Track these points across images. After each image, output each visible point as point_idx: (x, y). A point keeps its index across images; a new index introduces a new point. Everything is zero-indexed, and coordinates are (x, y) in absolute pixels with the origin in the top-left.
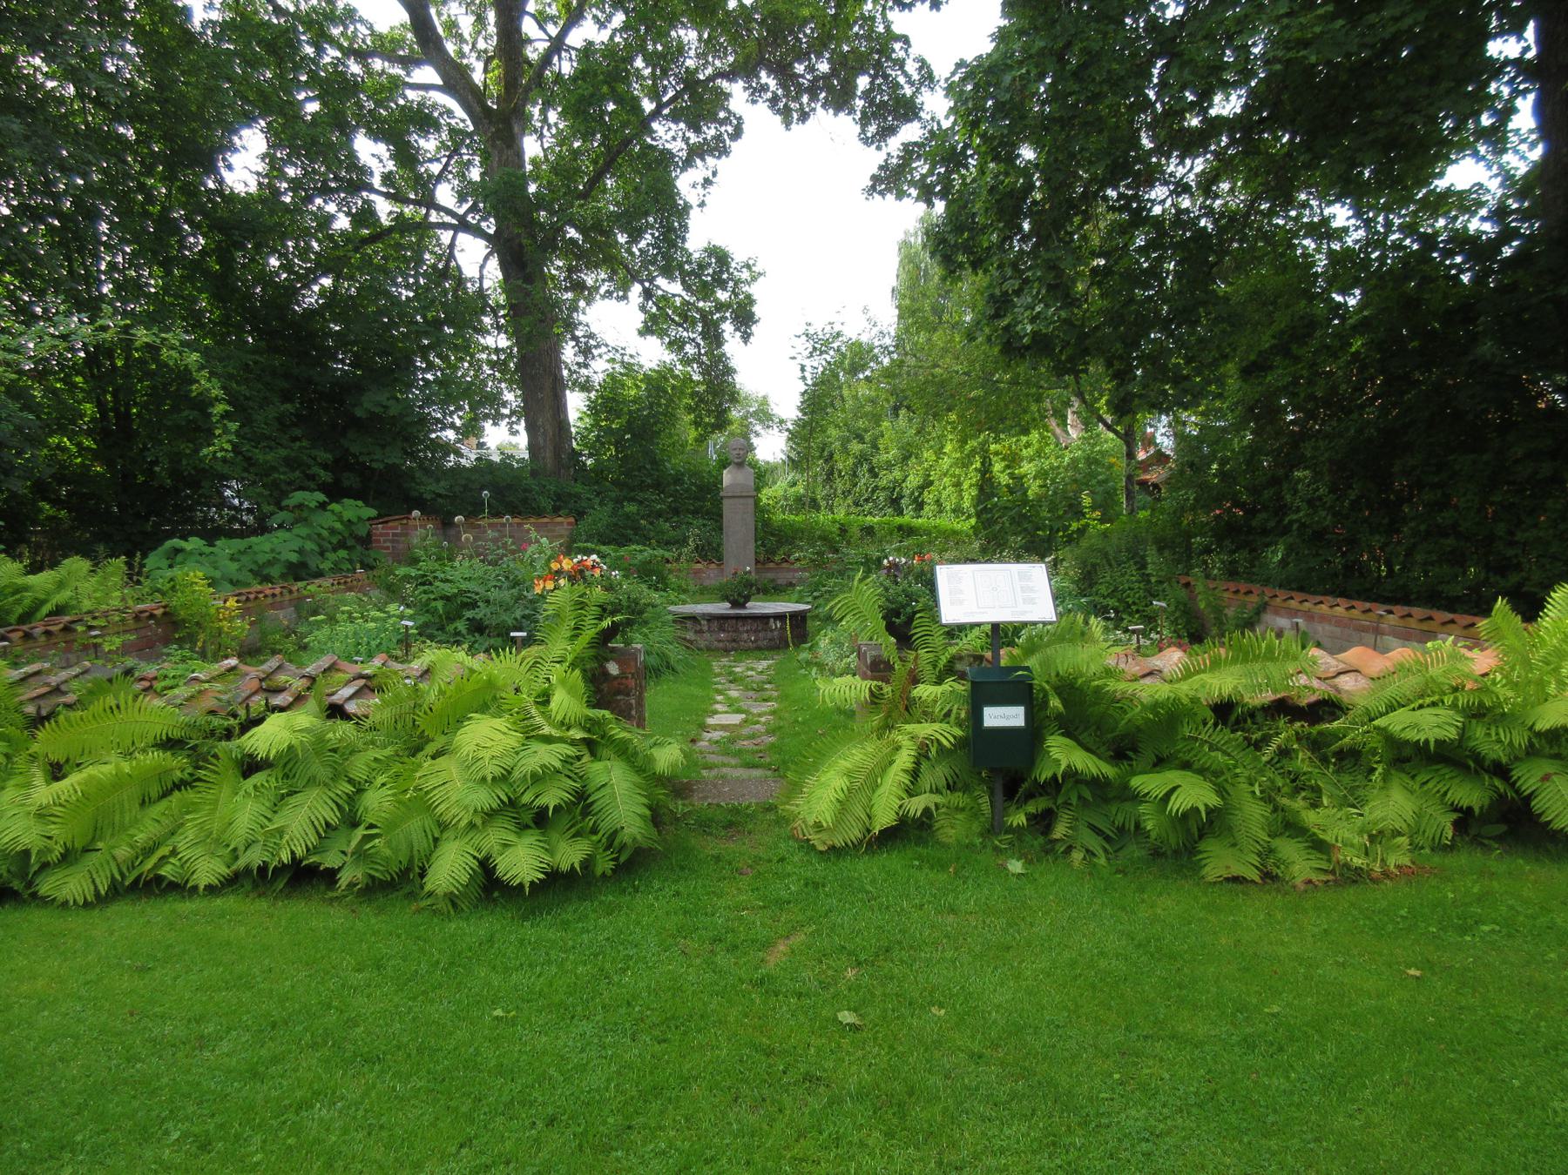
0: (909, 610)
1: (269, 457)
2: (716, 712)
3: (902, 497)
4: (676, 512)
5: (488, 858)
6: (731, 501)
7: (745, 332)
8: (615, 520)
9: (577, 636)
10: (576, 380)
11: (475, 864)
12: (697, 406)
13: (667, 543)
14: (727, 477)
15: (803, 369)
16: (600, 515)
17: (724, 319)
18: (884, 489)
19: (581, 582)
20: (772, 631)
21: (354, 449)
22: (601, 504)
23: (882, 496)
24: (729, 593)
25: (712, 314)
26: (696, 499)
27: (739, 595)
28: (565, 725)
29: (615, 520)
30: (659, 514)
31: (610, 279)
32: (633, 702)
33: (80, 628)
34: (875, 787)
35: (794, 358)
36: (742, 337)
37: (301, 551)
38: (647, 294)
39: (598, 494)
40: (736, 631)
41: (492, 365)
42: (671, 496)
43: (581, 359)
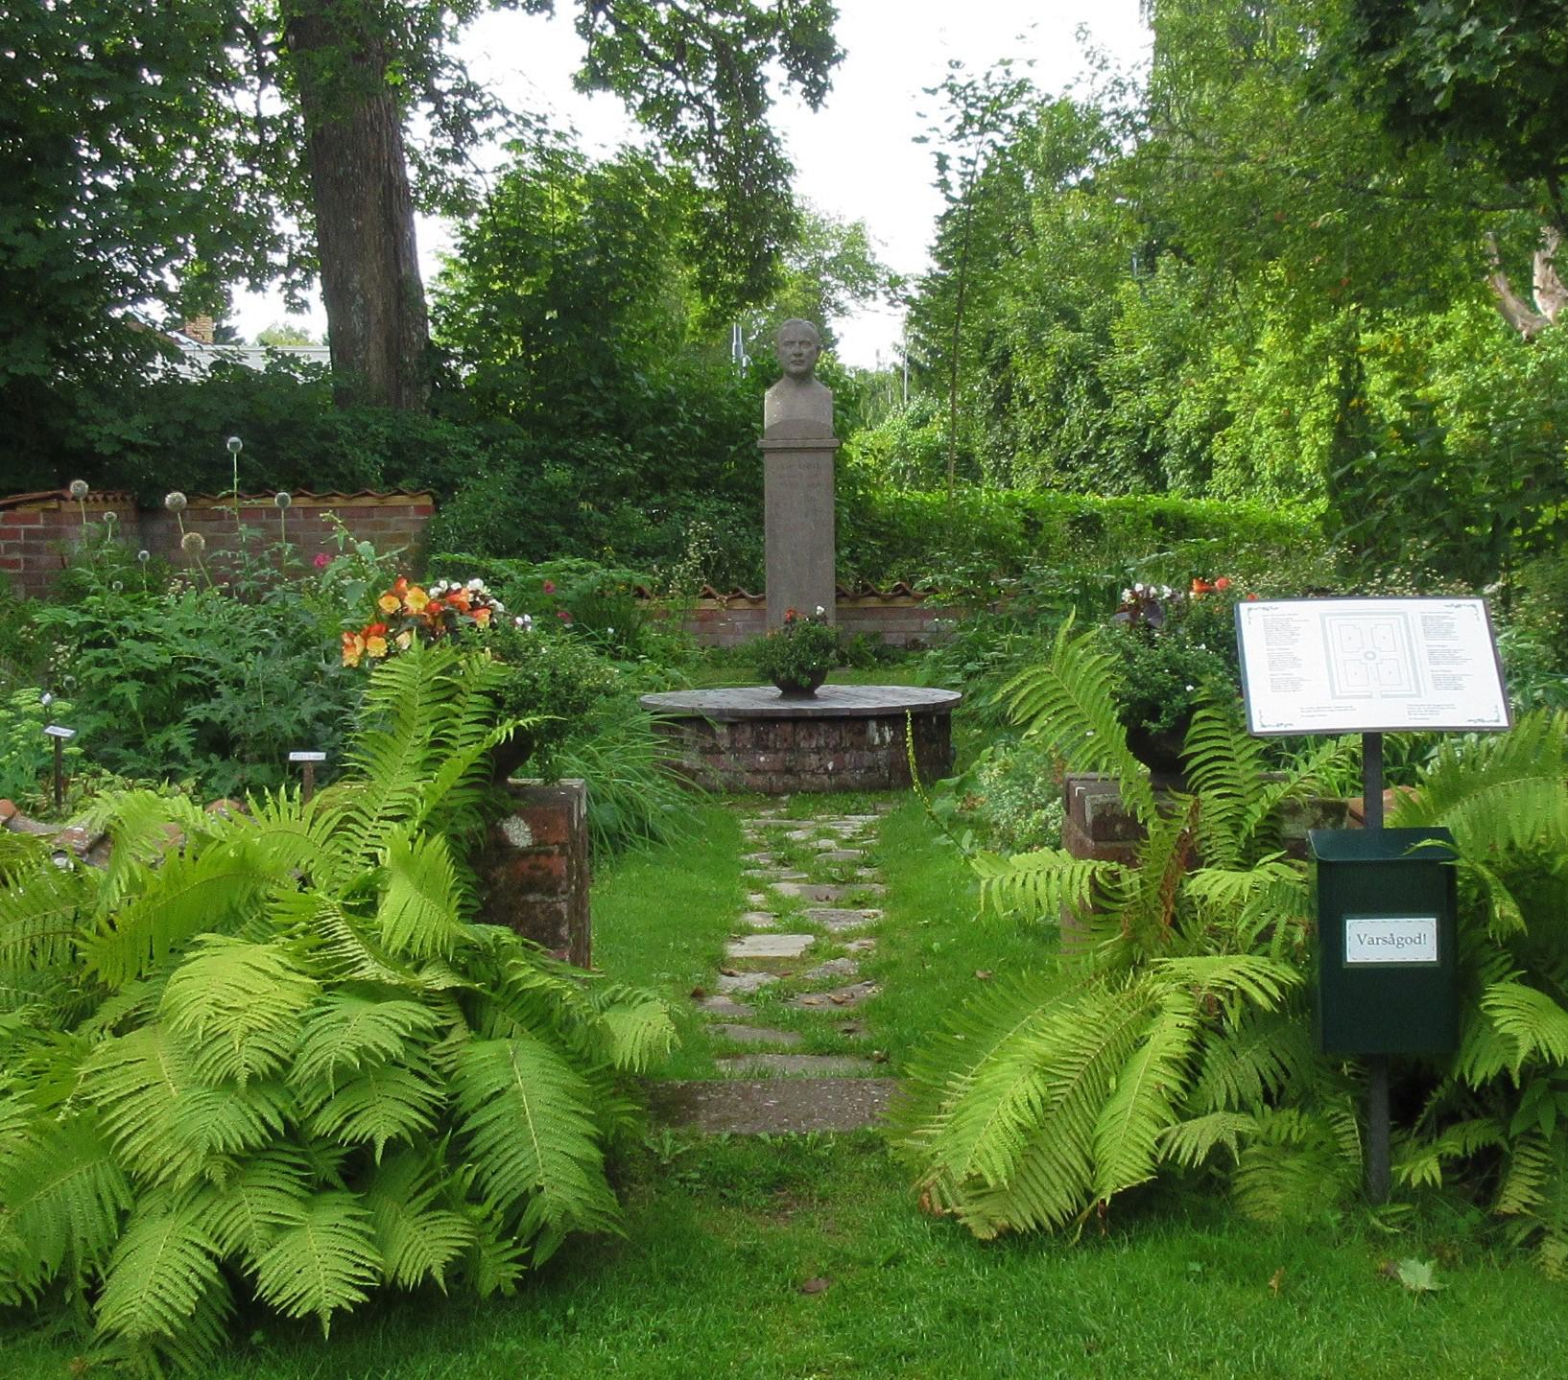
0: (1179, 701)
2: (749, 931)
3: (1164, 450)
4: (660, 483)
6: (784, 459)
7: (814, 82)
8: (522, 501)
9: (437, 760)
10: (436, 189)
12: (706, 246)
13: (640, 553)
14: (774, 405)
15: (942, 164)
17: (765, 53)
18: (1123, 431)
20: (873, 749)
22: (492, 465)
23: (1118, 448)
24: (777, 664)
25: (739, 40)
27: (800, 668)
28: (411, 959)
30: (622, 489)
32: (563, 907)
34: (1103, 1097)
35: (922, 140)
36: (807, 93)
39: (486, 443)
40: (793, 748)
41: (249, 154)
42: (649, 447)
43: (446, 142)
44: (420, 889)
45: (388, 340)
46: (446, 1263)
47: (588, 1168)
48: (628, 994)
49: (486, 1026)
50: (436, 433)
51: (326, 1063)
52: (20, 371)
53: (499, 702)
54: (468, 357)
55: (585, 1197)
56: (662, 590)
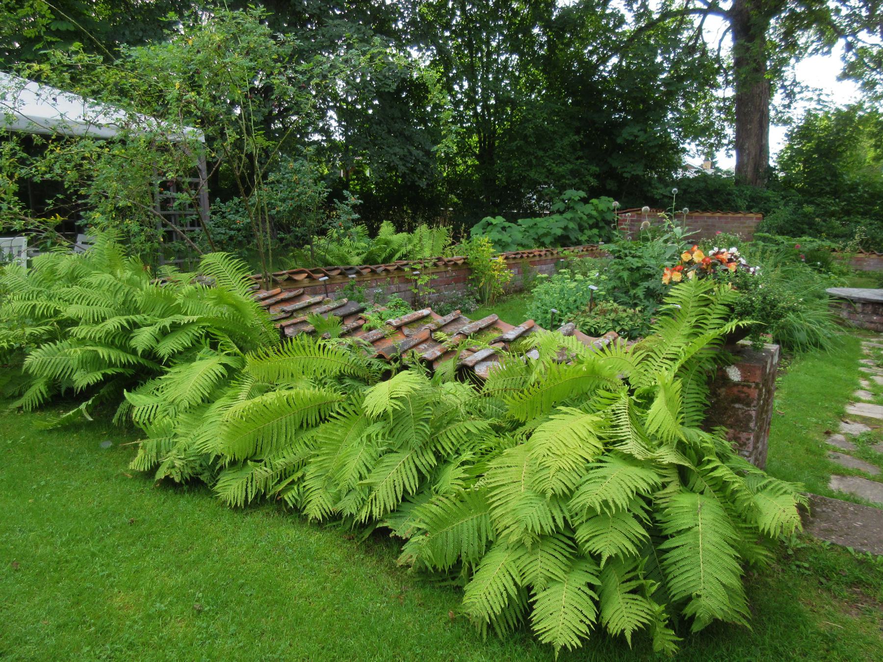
1: (561, 169)
2: (858, 400)
4: (848, 213)
5: (529, 588)
8: (795, 217)
9: (696, 335)
11: (513, 591)
13: (836, 236)
16: (783, 213)
19: (711, 276)
21: (615, 164)
26: (867, 203)
28: (655, 440)
29: (795, 217)
30: (833, 214)
31: (819, 39)
32: (753, 413)
33: (406, 269)
37: (565, 228)
38: (849, 46)
39: (784, 198)
41: (720, 109)
42: (845, 200)
43: (787, 102)
44: (667, 405)
45: (755, 165)
46: (634, 630)
47: (731, 593)
48: (776, 486)
49: (690, 485)
50: (767, 194)
51: (585, 505)
52: (635, 173)
53: (732, 310)
54: (782, 170)
55: (725, 609)
56: (843, 249)
